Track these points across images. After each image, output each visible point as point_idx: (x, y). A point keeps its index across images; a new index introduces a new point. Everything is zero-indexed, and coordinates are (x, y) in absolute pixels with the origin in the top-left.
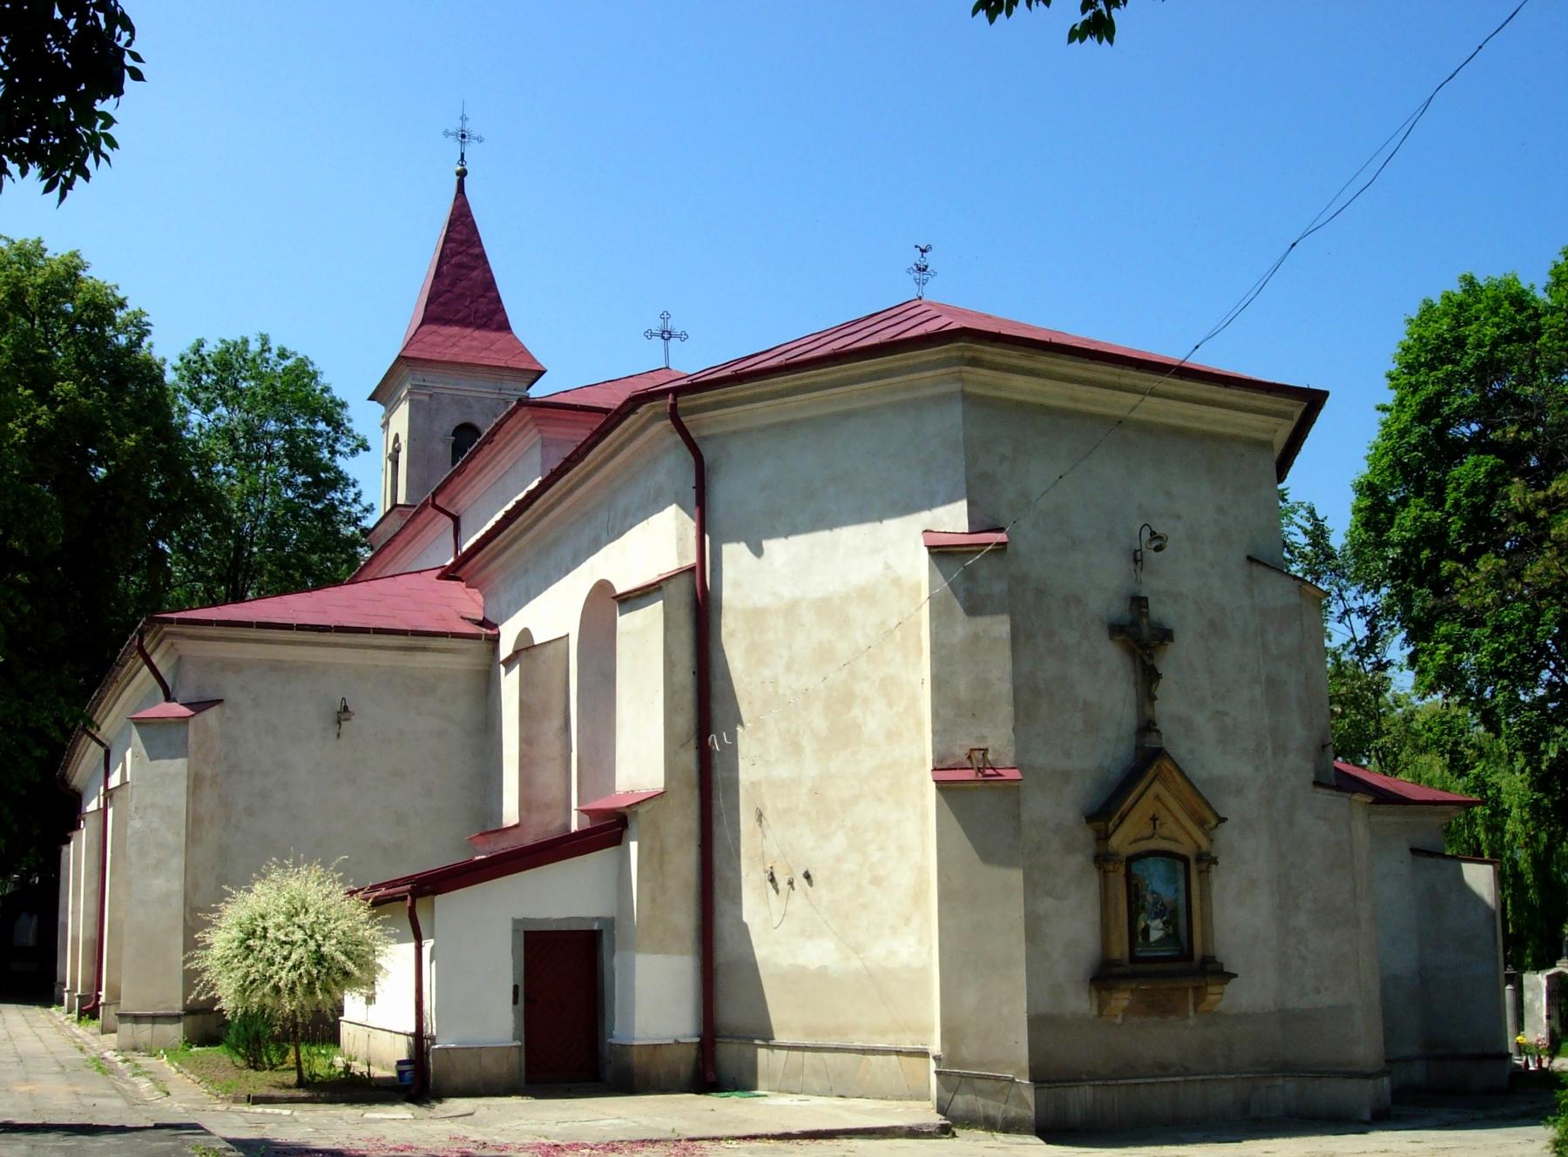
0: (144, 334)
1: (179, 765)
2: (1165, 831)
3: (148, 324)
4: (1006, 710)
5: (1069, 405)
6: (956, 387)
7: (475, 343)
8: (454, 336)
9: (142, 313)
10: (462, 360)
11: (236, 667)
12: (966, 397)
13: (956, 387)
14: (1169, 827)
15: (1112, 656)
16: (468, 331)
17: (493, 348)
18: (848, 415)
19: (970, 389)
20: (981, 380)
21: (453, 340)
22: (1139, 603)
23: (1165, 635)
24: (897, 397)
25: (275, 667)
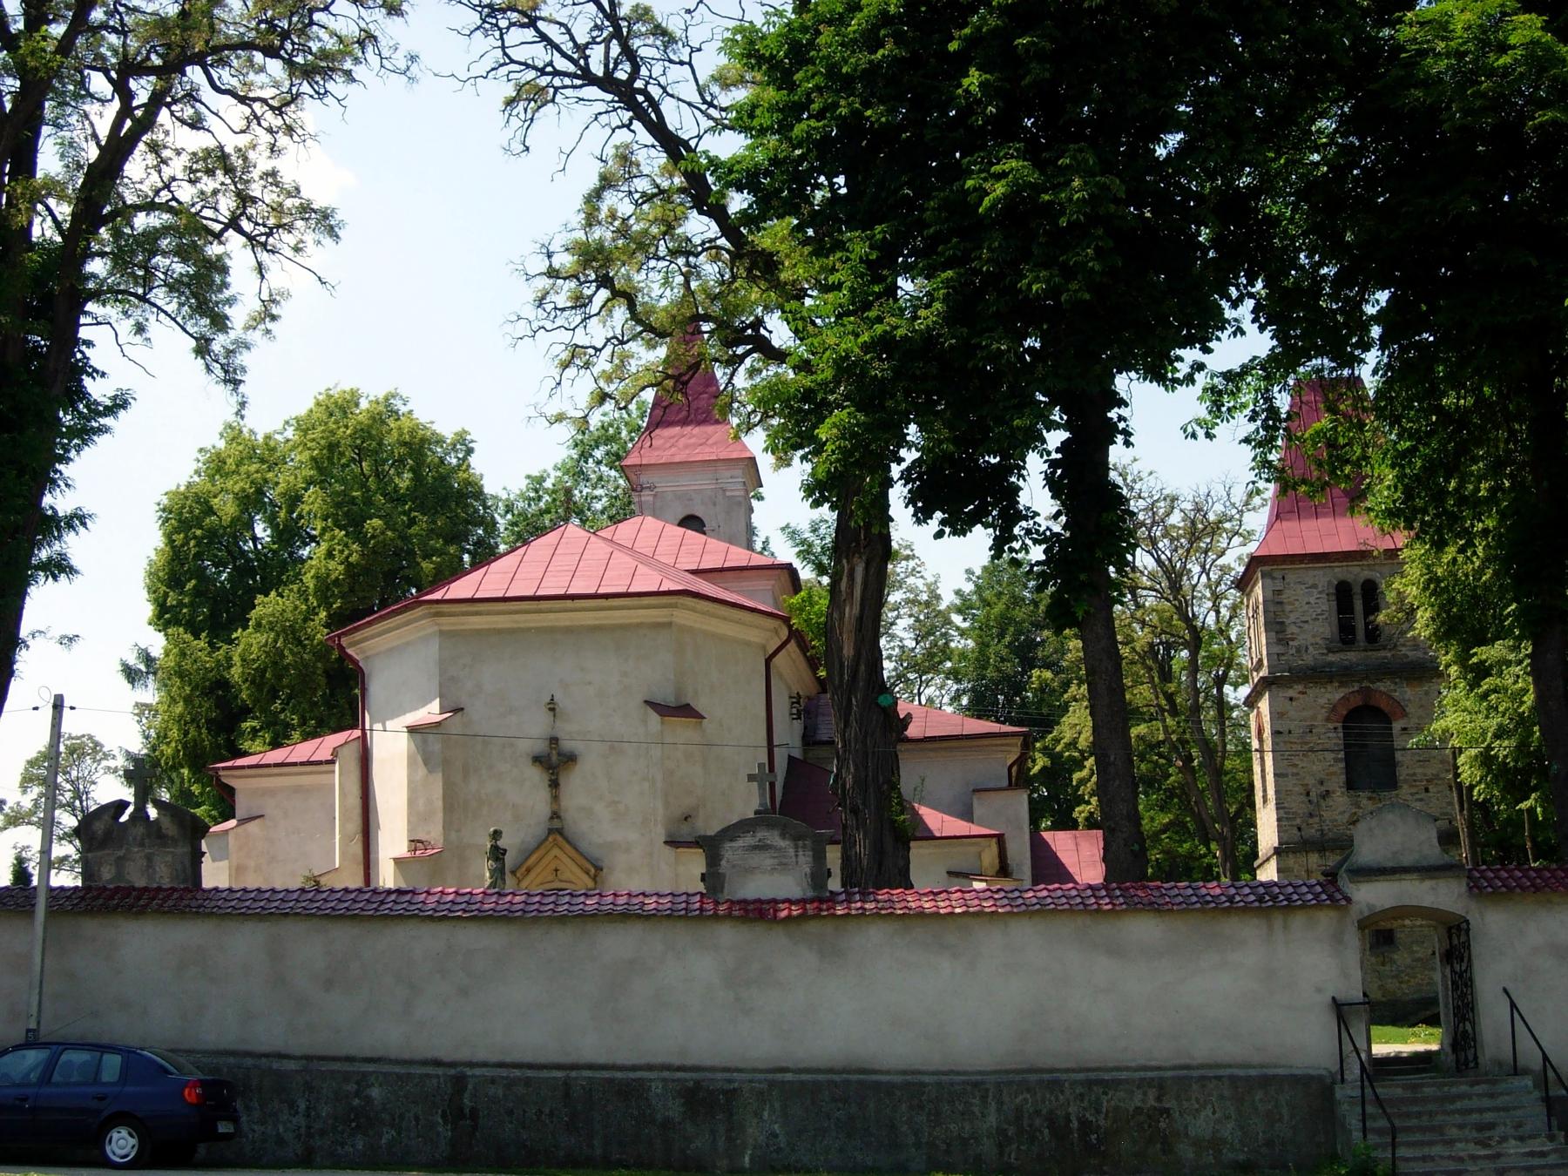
0: (470, 451)
1: (225, 864)
2: (563, 878)
3: (472, 441)
4: (439, 816)
5: (515, 626)
6: (436, 628)
7: (693, 440)
8: (673, 437)
9: (465, 432)
10: (677, 459)
11: (271, 792)
12: (442, 633)
13: (436, 628)
14: (566, 875)
15: (536, 778)
16: (688, 429)
17: (710, 442)
18: (408, 644)
19: (445, 628)
20: (447, 623)
21: (672, 441)
22: (554, 741)
23: (570, 759)
24: (422, 633)
25: (298, 789)
